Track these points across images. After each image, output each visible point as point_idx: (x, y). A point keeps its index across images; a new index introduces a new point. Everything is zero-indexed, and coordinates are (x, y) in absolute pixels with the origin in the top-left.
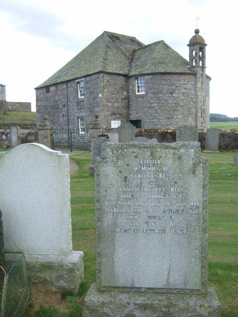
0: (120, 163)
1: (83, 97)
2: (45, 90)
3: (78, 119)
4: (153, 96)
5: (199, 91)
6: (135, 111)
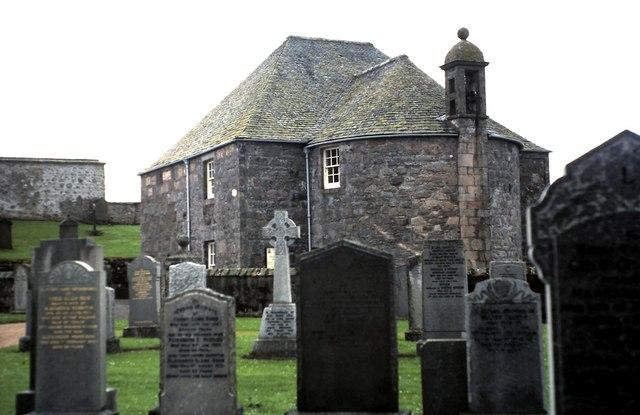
2: (154, 178)
3: (206, 246)
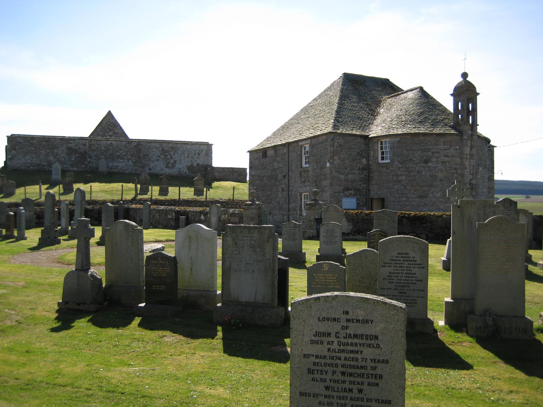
0: (234, 235)
1: (307, 165)
4: (400, 166)
5: (467, 159)
6: (376, 186)
